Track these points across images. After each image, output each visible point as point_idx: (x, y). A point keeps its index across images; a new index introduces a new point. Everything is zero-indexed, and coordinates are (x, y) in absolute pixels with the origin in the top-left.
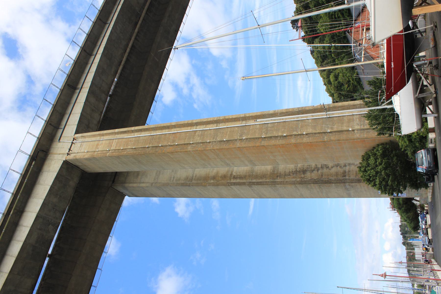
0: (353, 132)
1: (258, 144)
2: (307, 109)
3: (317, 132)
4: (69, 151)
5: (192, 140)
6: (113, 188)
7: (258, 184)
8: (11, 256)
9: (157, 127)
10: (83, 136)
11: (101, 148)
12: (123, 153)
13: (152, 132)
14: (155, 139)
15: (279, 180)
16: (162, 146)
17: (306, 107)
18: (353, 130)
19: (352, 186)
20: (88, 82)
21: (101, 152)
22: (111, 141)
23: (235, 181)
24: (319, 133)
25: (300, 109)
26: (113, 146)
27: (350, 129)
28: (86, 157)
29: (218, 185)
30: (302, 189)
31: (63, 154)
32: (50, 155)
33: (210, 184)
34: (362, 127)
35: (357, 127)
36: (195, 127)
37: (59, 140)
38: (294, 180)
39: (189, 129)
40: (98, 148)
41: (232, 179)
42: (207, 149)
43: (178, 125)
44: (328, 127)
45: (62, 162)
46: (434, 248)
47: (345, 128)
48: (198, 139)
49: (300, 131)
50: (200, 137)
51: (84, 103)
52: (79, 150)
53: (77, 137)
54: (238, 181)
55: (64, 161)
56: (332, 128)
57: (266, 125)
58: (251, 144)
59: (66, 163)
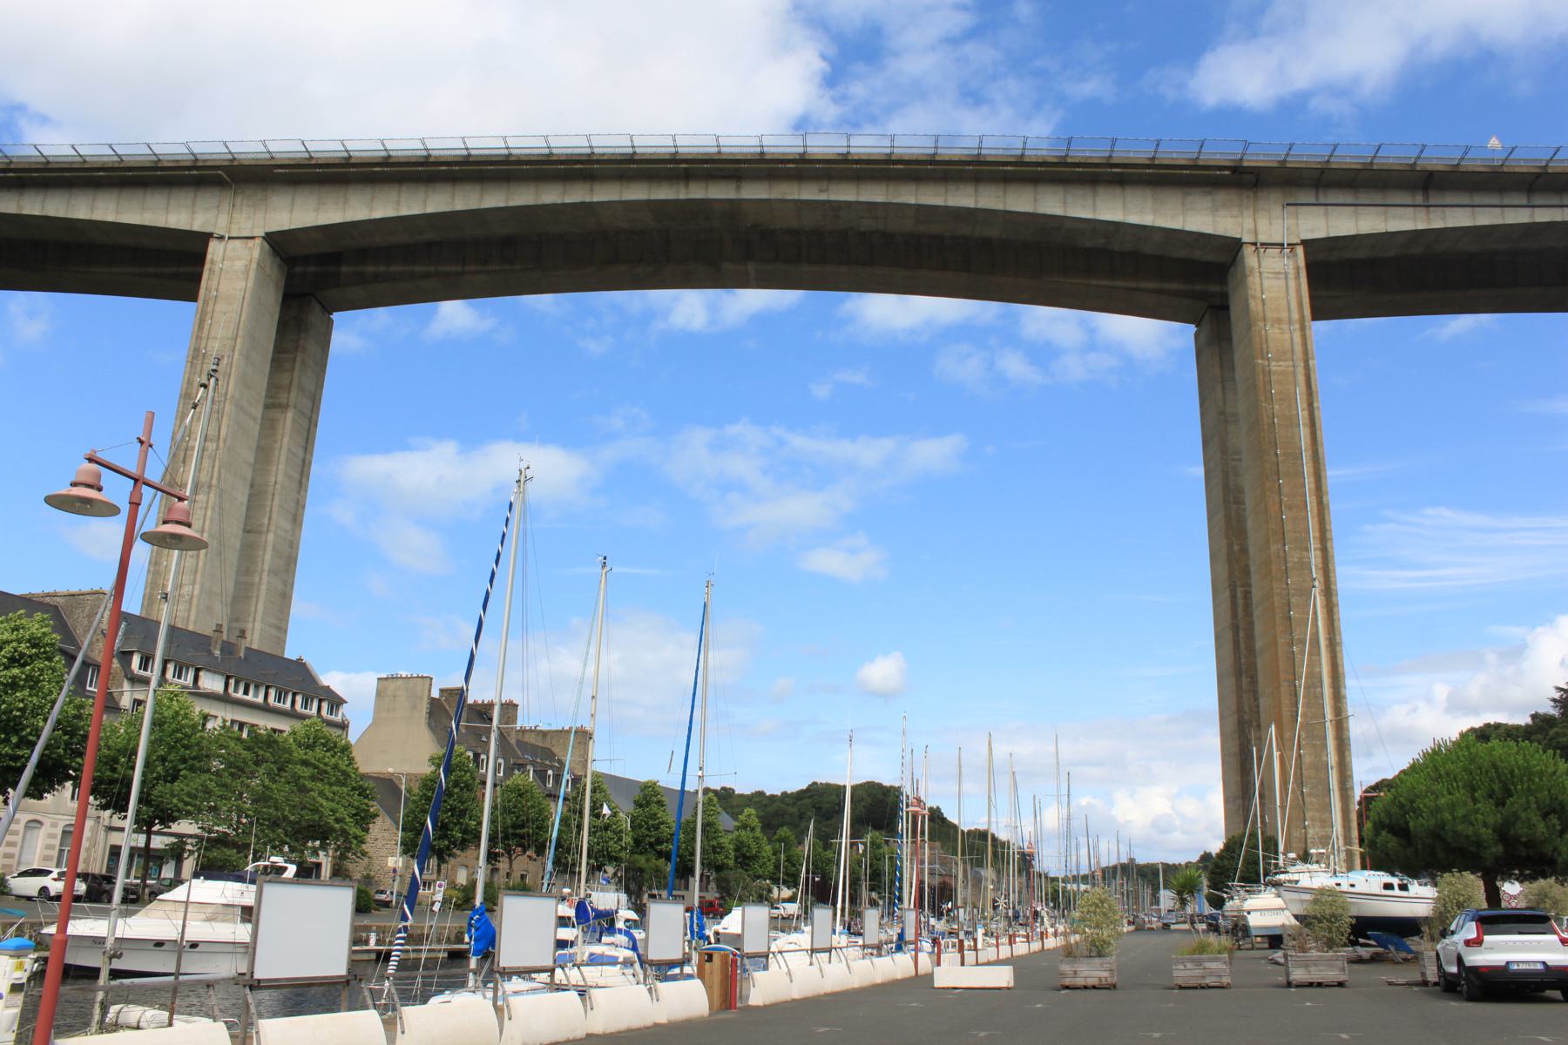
0: (1302, 826)
1: (1282, 676)
2: (1347, 753)
3: (1304, 772)
4: (1262, 244)
5: (1292, 546)
6: (1205, 313)
7: (1236, 643)
8: (1035, 200)
9: (1319, 463)
10: (1298, 273)
11: (1273, 332)
12: (1263, 398)
13: (1310, 453)
14: (1294, 464)
15: (1245, 681)
16: (1279, 485)
17: (1350, 750)
18: (1305, 828)
19: (1238, 809)
20: (1444, 219)
21: (1264, 337)
22: (1289, 355)
23: (1239, 595)
24: (1302, 774)
25: (1346, 741)
26: (1280, 363)
27: (1307, 823)
28: (1252, 304)
29: (1229, 562)
30: (1232, 720)
31: (1256, 233)
32: (1251, 194)
33: (1230, 546)
34: (1309, 841)
35: (1311, 832)
36: (1319, 546)
37: (1288, 204)
38: (1246, 709)
39: (1313, 533)
40: (1272, 326)
41: (1242, 589)
42: (1274, 583)
43: (1324, 509)
44: (1312, 788)
45: (1238, 236)
46: (49, 961)
47: (1308, 815)
48: (1293, 558)
49: (1307, 744)
50: (1298, 562)
51: (1384, 231)
52: (1268, 272)
53: (1296, 255)
54: (1240, 602)
55: (1240, 239)
56: (1310, 794)
57: (1319, 684)
58: (1282, 664)
59: (1233, 247)
